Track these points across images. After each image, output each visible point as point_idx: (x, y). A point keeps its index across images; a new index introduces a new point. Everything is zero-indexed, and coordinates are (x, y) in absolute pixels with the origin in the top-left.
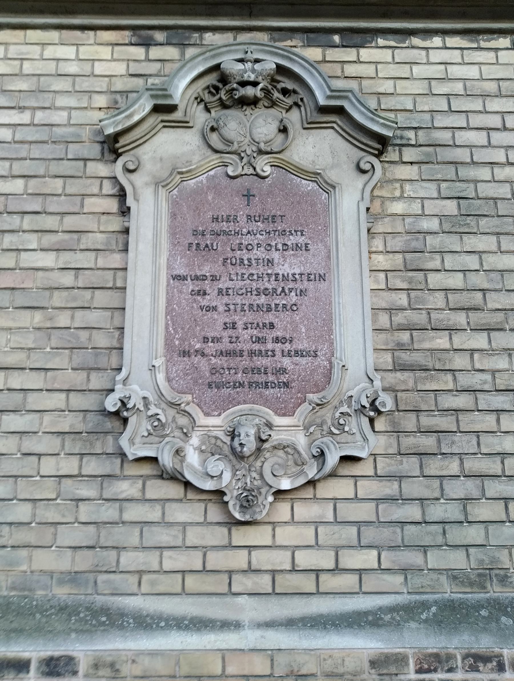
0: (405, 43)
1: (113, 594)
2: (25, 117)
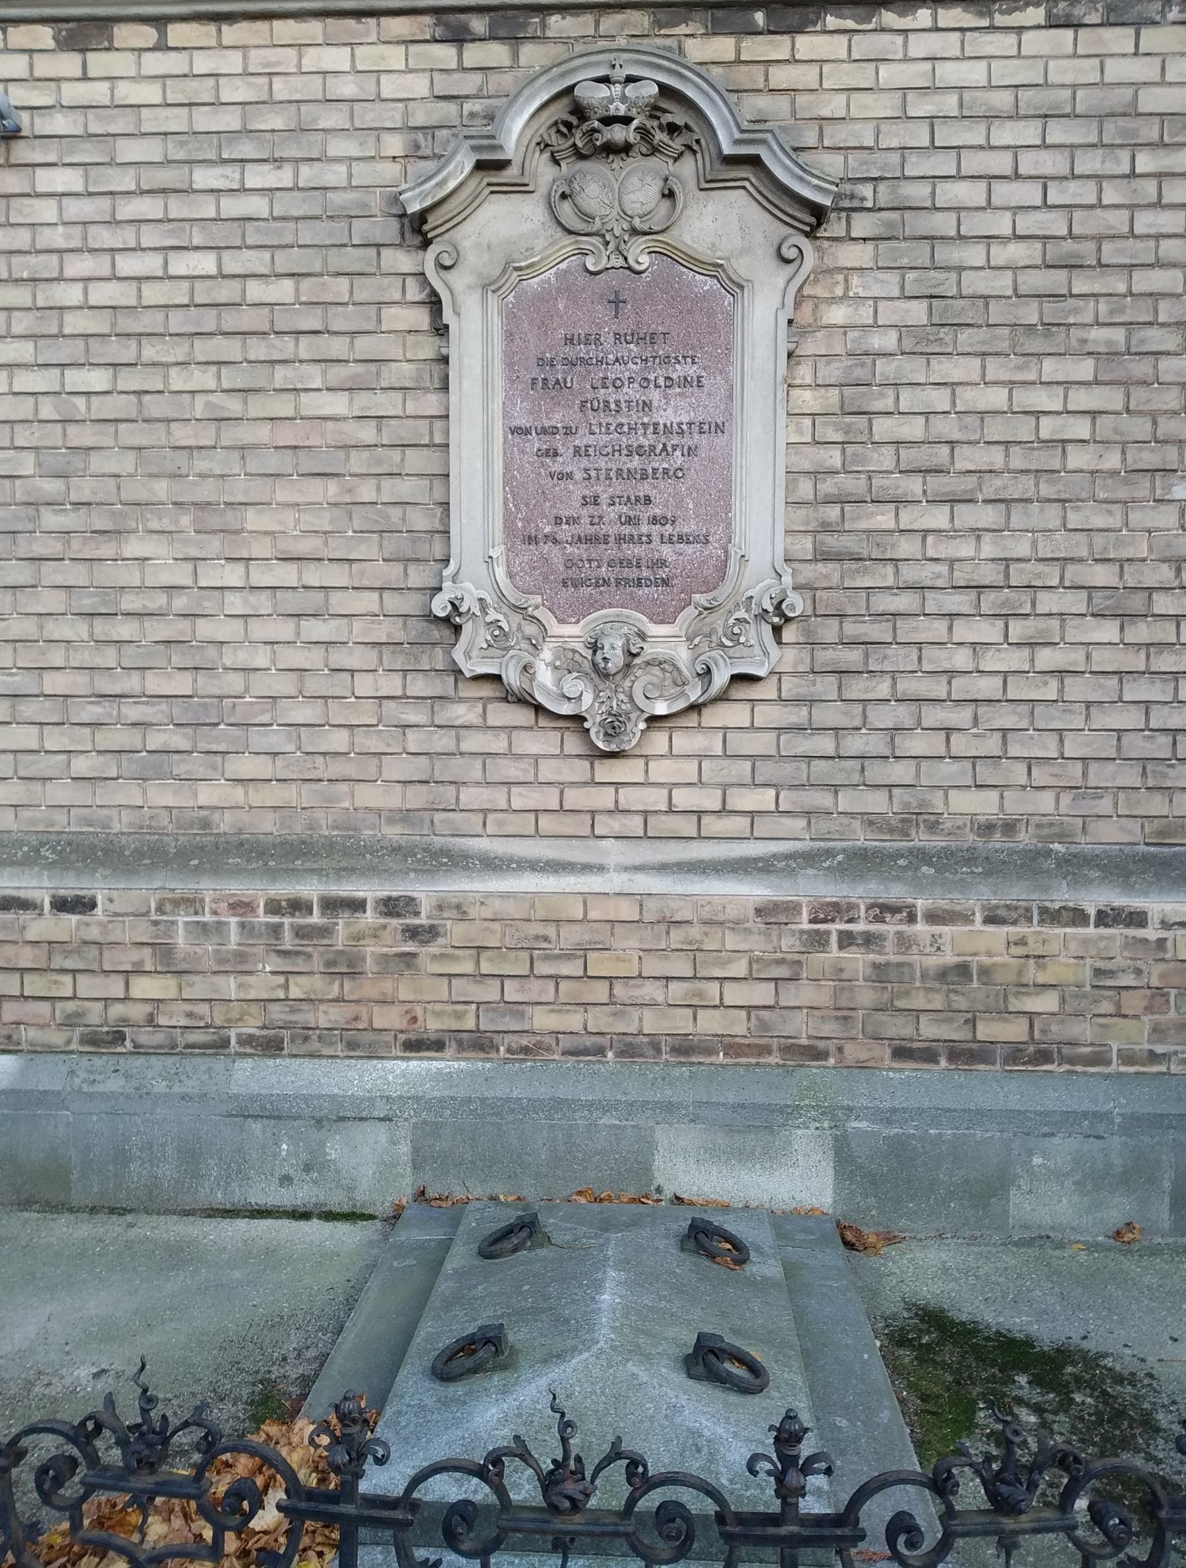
0: (870, 22)
1: (453, 835)
2: (284, 177)
